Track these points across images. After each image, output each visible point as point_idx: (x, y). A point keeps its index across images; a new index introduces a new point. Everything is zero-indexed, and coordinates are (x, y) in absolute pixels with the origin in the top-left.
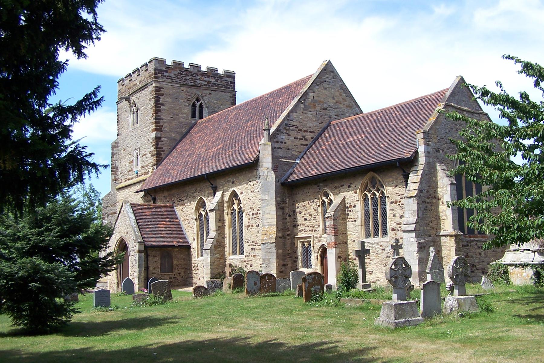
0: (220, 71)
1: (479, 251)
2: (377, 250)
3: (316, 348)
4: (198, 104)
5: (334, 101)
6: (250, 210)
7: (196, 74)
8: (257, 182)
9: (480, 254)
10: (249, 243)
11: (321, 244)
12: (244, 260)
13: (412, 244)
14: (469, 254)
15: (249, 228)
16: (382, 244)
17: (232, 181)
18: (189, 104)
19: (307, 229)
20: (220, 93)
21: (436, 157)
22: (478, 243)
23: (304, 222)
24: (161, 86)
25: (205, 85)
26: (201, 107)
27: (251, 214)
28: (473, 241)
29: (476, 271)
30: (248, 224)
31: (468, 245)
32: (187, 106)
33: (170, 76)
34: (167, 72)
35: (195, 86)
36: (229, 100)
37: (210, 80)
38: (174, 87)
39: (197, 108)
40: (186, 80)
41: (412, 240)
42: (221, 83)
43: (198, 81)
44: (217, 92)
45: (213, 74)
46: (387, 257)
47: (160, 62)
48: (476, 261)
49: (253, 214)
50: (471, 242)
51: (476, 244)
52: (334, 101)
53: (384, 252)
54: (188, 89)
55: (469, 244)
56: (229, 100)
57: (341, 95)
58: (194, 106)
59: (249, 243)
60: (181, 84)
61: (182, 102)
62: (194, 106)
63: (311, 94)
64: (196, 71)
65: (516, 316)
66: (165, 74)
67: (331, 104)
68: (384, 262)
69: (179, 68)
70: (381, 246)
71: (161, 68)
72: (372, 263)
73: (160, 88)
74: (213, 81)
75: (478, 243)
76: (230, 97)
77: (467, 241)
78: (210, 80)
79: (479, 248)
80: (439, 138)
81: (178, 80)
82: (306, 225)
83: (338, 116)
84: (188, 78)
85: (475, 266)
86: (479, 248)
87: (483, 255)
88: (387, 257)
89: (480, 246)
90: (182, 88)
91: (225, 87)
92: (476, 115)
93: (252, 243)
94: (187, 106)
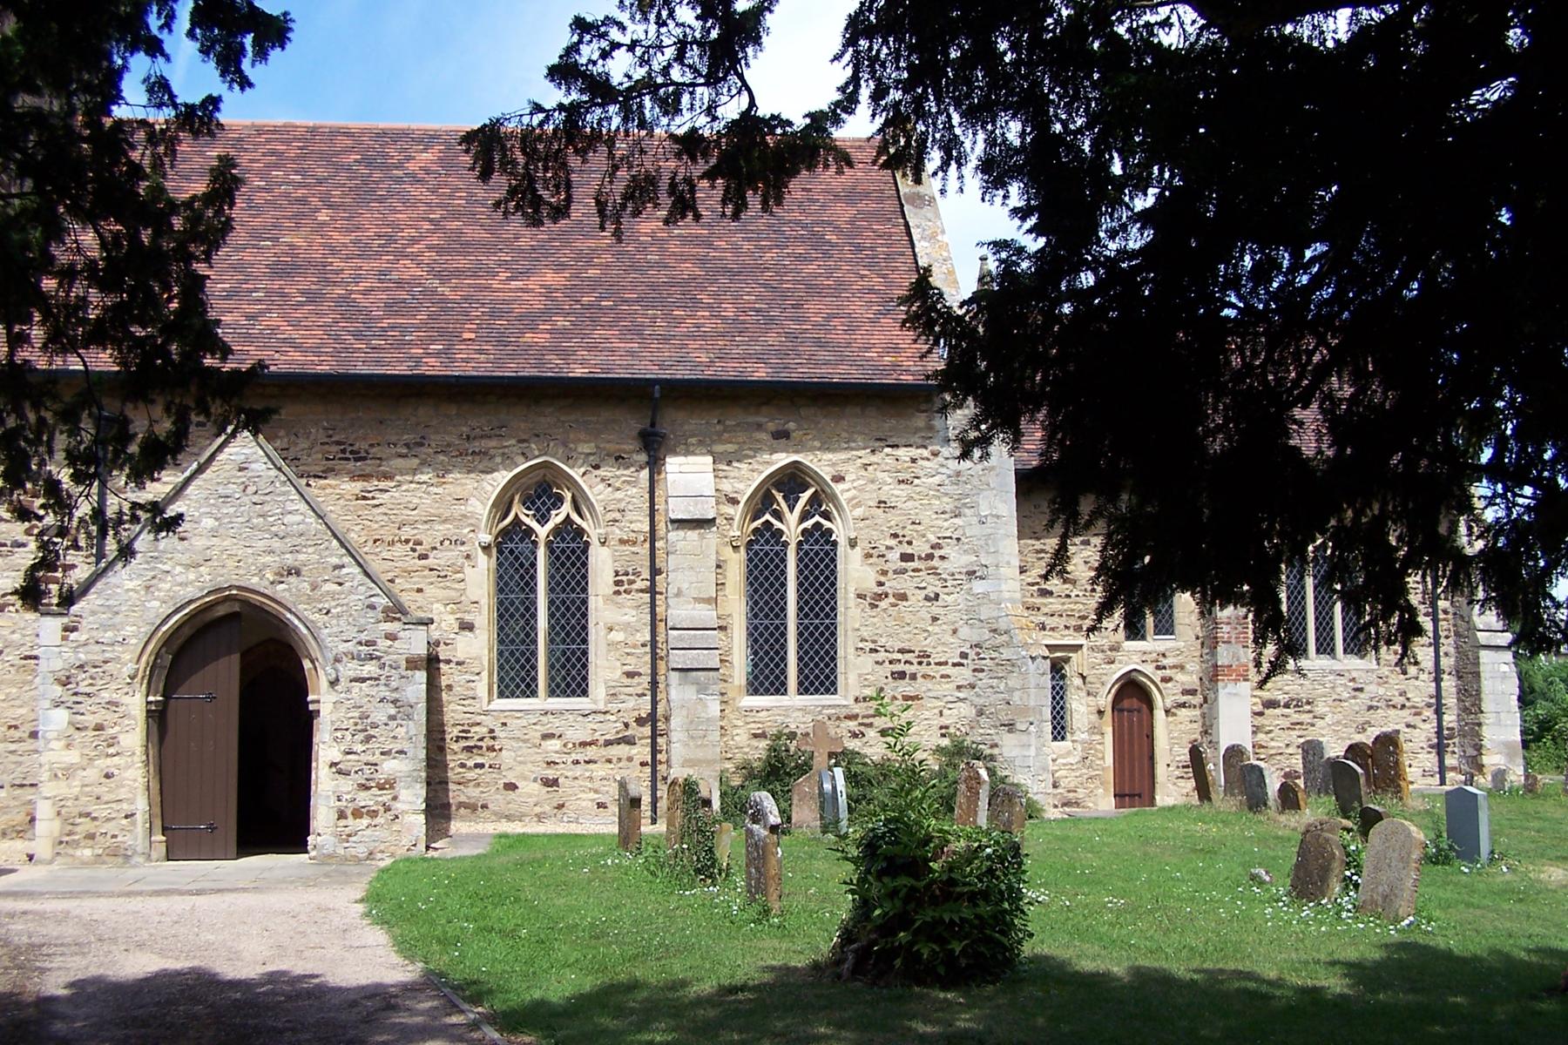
2: (1339, 690)
3: (629, 1038)
6: (893, 542)
8: (935, 454)
10: (882, 656)
11: (1119, 670)
12: (844, 712)
13: (1504, 676)
15: (883, 604)
16: (1354, 674)
17: (771, 426)
19: (1062, 622)
23: (1039, 601)
27: (894, 556)
30: (879, 590)
41: (1505, 668)
46: (1370, 708)
49: (906, 557)
53: (1361, 695)
59: (882, 656)
68: (1361, 720)
70: (1353, 680)
72: (1319, 723)
82: (1045, 610)
88: (1370, 708)
93: (899, 656)
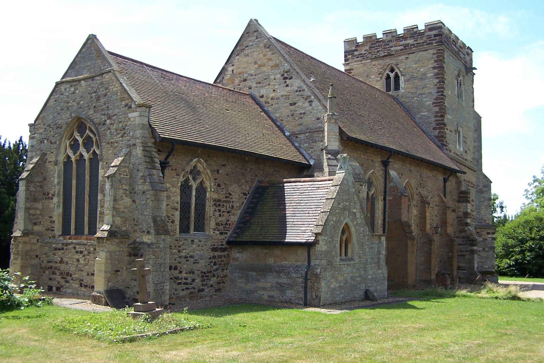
0: (421, 27)
1: (77, 256)
4: (392, 75)
5: (256, 66)
7: (391, 41)
9: (78, 260)
14: (64, 259)
18: (381, 78)
20: (420, 53)
21: (40, 149)
22: (77, 247)
24: (351, 67)
25: (401, 50)
26: (397, 77)
28: (69, 244)
29: (72, 281)
31: (63, 249)
32: (379, 81)
33: (361, 54)
34: (356, 50)
35: (390, 55)
36: (432, 58)
37: (407, 42)
38: (365, 64)
39: (392, 79)
40: (378, 52)
42: (421, 42)
43: (392, 49)
44: (416, 53)
45: (411, 34)
47: (350, 43)
48: (72, 269)
50: (67, 244)
51: (75, 248)
52: (256, 66)
54: (381, 62)
55: (65, 248)
56: (432, 58)
57: (265, 55)
58: (388, 77)
60: (371, 59)
61: (374, 78)
62: (388, 77)
63: (230, 69)
64: (390, 37)
65: (123, 341)
66: (356, 53)
67: (252, 72)
69: (370, 42)
71: (351, 49)
73: (350, 70)
74: (410, 41)
75: (77, 247)
76: (434, 54)
77: (63, 244)
78: (407, 42)
79: (77, 252)
80: (45, 127)
81: (369, 56)
83: (259, 83)
84: (381, 49)
85: (71, 275)
86: (77, 252)
87: (82, 261)
89: (79, 250)
90: (373, 63)
91: (427, 45)
92: (98, 78)
94: (379, 81)
